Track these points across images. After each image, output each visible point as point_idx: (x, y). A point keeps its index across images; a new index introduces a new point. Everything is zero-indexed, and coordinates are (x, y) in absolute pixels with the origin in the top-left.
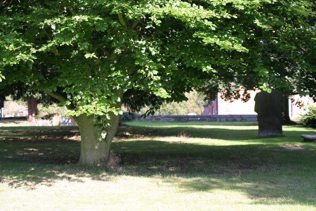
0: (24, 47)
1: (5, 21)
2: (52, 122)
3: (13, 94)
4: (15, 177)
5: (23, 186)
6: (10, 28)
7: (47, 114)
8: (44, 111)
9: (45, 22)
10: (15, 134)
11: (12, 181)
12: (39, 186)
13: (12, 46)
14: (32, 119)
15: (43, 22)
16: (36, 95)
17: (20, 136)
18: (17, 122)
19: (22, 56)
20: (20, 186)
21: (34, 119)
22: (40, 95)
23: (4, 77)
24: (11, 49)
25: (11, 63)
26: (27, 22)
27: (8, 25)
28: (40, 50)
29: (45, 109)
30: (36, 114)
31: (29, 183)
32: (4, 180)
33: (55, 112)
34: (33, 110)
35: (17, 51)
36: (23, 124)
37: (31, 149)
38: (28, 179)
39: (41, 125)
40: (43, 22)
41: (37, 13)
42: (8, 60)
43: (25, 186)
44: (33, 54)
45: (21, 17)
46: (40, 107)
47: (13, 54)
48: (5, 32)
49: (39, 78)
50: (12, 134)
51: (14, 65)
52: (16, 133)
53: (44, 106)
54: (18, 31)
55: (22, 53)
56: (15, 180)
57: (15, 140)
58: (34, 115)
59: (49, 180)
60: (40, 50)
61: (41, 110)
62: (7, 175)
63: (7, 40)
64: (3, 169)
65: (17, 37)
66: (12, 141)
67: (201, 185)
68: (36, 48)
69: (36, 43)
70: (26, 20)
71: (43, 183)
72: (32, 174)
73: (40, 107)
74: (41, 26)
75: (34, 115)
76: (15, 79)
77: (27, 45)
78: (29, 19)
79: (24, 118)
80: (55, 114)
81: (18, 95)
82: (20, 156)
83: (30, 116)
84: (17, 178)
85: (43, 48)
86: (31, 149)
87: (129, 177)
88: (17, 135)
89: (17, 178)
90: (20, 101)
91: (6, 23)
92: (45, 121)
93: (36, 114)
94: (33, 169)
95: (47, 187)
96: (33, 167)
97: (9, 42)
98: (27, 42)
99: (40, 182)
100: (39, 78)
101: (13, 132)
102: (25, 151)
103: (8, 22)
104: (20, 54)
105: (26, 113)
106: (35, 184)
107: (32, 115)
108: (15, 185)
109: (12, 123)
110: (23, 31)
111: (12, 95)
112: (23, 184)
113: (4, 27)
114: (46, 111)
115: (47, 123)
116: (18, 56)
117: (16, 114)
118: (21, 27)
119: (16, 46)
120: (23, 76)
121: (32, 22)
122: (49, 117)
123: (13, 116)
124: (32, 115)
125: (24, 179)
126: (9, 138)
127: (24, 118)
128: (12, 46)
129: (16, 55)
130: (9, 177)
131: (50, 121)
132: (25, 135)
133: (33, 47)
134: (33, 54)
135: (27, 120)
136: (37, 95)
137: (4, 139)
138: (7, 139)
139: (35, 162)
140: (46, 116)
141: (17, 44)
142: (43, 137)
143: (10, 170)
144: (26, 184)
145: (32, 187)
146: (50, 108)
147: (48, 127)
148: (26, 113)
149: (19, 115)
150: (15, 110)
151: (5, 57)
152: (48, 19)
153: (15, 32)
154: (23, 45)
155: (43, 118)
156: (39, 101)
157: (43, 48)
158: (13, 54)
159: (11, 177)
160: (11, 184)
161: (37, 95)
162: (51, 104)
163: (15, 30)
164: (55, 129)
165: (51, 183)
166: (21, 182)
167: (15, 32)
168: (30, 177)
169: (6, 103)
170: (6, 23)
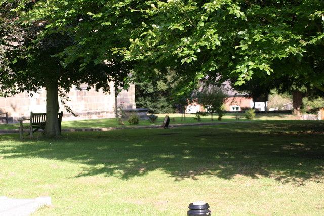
0: (293, 39)
1: (273, 13)
2: (317, 116)
3: (278, 87)
4: (282, 172)
5: (291, 182)
6: (279, 20)
7: (311, 108)
8: (309, 105)
9: (316, 13)
10: (280, 128)
11: (279, 176)
12: (307, 182)
13: (281, 38)
14: (297, 113)
15: (313, 13)
16: (302, 88)
17: (285, 130)
18: (282, 115)
19: (292, 49)
20: (288, 182)
21: (299, 113)
22: (306, 88)
23: (272, 71)
24: (280, 42)
25: (280, 56)
26: (297, 13)
27: (276, 17)
28: (310, 42)
29: (310, 102)
30: (302, 108)
31: (298, 179)
32: (272, 174)
33: (320, 106)
34: (298, 104)
35: (286, 43)
36: (289, 118)
37: (298, 144)
38: (297, 175)
39: (305, 119)
40: (313, 13)
41: (307, 4)
42: (277, 52)
43: (293, 182)
44: (303, 47)
45: (290, 8)
46: (305, 100)
47: (282, 46)
48: (273, 24)
49: (308, 71)
50: (277, 128)
51: (283, 58)
52: (281, 126)
53: (310, 100)
54: (288, 23)
55: (291, 45)
56: (282, 175)
57: (281, 135)
58: (299, 109)
59: (318, 176)
60: (310, 42)
61: (306, 104)
62: (274, 170)
63: (276, 32)
64: (270, 163)
65: (286, 29)
66: (277, 135)
67: (86, 172)
68: (305, 41)
69: (305, 36)
70: (296, 12)
71: (311, 179)
72: (299, 169)
73: (305, 100)
74: (312, 17)
75: (299, 109)
76: (284, 73)
77: (296, 38)
78: (298, 11)
79: (289, 112)
80: (321, 108)
81: (283, 88)
82: (287, 150)
83: (295, 110)
84: (284, 173)
85: (314, 41)
86: (298, 144)
87: (40, 159)
88: (281, 129)
89: (284, 173)
90: (285, 94)
91: (275, 15)
92: (311, 115)
93: (302, 108)
94: (300, 164)
95: (316, 184)
96: (301, 162)
97: (277, 34)
98: (297, 35)
99: (308, 178)
100: (308, 71)
101: (278, 126)
102: (291, 145)
103: (277, 13)
104: (289, 46)
105: (290, 107)
106: (304, 180)
107: (297, 109)
108: (283, 180)
109: (276, 117)
110: (292, 23)
111: (277, 88)
112: (291, 180)
113: (273, 19)
114: (311, 105)
115: (312, 117)
116: (287, 49)
117: (280, 107)
118: (290, 19)
119: (284, 38)
120: (291, 69)
121: (301, 14)
122: (315, 111)
123: (277, 110)
124: (297, 109)
125: (291, 174)
126: (274, 132)
127: (289, 112)
128: (281, 38)
129: (286, 48)
130: (276, 172)
131: (316, 116)
132: (290, 129)
133: (302, 39)
134: (303, 47)
135: (292, 114)
136: (303, 88)
137: (269, 133)
138: (272, 132)
139: (302, 157)
140: (312, 110)
141: (286, 37)
142: (309, 132)
143: (277, 164)
144: (294, 180)
145: (300, 183)
146: (316, 102)
147: (314, 121)
148: (290, 107)
149: (283, 109)
150: (280, 102)
151: (273, 50)
152: (319, 10)
153: (284, 24)
154: (292, 37)
155: (308, 113)
156: (303, 95)
157: (314, 41)
158: (282, 46)
159: (278, 172)
160: (279, 179)
161: (303, 88)
162: (317, 98)
163: (285, 21)
164: (321, 123)
165: (319, 180)
166: (289, 177)
167: (284, 24)
168: (297, 173)
169: (270, 96)
170: (275, 15)
